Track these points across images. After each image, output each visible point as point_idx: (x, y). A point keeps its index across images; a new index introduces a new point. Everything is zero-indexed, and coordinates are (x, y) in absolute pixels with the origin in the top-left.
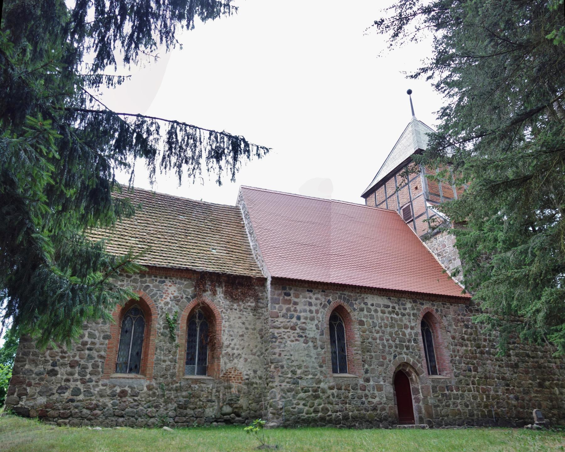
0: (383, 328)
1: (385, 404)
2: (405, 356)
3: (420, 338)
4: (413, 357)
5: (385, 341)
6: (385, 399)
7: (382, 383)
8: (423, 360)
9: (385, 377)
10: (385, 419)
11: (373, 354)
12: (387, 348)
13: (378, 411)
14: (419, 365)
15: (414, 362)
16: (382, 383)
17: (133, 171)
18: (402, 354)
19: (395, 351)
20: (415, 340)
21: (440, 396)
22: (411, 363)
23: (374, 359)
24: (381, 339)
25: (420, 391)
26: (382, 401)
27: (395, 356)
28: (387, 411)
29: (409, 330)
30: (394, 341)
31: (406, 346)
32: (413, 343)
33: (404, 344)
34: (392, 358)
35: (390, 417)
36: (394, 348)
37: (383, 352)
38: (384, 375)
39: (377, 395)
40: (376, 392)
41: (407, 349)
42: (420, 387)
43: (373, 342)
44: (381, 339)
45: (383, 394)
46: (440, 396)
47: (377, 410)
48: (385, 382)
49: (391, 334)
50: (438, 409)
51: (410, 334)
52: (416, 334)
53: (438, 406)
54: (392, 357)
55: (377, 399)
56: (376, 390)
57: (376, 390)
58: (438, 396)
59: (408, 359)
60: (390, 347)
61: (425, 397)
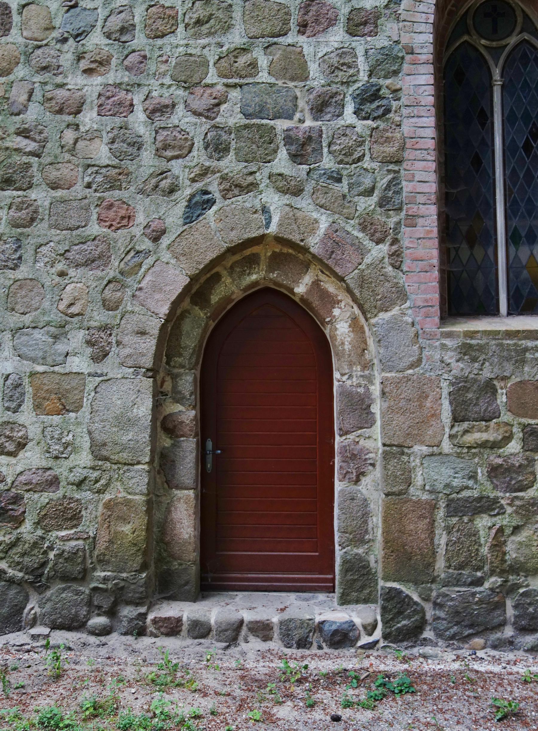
0: (139, 40)
1: (79, 484)
2: (275, 201)
3: (419, 84)
4: (340, 206)
5: (139, 116)
6: (84, 458)
7: (79, 364)
8: (412, 220)
9: (104, 328)
10: (74, 571)
11: (40, 196)
12: (147, 158)
13: (27, 527)
14: (379, 251)
15: (335, 241)
16: (79, 364)
17: (5, 381)
18: (252, 187)
19: (205, 172)
20: (369, 97)
21: (514, 446)
22: (314, 243)
23: (41, 228)
24: (114, 104)
25: (376, 409)
26: (61, 470)
27: (199, 205)
28: (89, 526)
29: (337, 37)
30: (210, 112)
31: (289, 140)
32: (136, 286)
33: (281, 125)
34: (174, 214)
35: (102, 561)
36: (199, 156)
37: (113, 184)
38: (99, 317)
39: (34, 431)
40: (27, 416)
41: (297, 157)
42: (376, 389)
43: (54, 123)
44: (114, 104)
45: (79, 427)
46: (514, 446)
47: (19, 521)
48: (100, 356)
49: (189, 77)
50: (483, 522)
51: (340, 64)
52: (390, 62)
53: (486, 506)
54: (180, 209)
55: (32, 458)
56: (28, 405)
57: (28, 405)
58: (494, 445)
59: (292, 216)
60: (173, 147)
61: (395, 450)
